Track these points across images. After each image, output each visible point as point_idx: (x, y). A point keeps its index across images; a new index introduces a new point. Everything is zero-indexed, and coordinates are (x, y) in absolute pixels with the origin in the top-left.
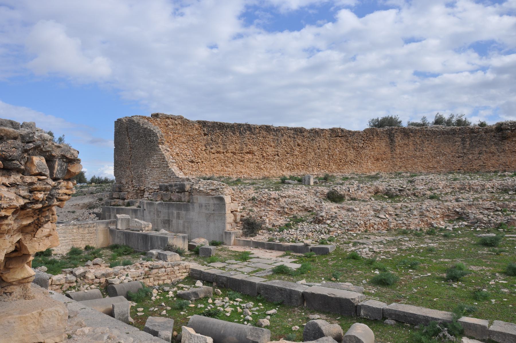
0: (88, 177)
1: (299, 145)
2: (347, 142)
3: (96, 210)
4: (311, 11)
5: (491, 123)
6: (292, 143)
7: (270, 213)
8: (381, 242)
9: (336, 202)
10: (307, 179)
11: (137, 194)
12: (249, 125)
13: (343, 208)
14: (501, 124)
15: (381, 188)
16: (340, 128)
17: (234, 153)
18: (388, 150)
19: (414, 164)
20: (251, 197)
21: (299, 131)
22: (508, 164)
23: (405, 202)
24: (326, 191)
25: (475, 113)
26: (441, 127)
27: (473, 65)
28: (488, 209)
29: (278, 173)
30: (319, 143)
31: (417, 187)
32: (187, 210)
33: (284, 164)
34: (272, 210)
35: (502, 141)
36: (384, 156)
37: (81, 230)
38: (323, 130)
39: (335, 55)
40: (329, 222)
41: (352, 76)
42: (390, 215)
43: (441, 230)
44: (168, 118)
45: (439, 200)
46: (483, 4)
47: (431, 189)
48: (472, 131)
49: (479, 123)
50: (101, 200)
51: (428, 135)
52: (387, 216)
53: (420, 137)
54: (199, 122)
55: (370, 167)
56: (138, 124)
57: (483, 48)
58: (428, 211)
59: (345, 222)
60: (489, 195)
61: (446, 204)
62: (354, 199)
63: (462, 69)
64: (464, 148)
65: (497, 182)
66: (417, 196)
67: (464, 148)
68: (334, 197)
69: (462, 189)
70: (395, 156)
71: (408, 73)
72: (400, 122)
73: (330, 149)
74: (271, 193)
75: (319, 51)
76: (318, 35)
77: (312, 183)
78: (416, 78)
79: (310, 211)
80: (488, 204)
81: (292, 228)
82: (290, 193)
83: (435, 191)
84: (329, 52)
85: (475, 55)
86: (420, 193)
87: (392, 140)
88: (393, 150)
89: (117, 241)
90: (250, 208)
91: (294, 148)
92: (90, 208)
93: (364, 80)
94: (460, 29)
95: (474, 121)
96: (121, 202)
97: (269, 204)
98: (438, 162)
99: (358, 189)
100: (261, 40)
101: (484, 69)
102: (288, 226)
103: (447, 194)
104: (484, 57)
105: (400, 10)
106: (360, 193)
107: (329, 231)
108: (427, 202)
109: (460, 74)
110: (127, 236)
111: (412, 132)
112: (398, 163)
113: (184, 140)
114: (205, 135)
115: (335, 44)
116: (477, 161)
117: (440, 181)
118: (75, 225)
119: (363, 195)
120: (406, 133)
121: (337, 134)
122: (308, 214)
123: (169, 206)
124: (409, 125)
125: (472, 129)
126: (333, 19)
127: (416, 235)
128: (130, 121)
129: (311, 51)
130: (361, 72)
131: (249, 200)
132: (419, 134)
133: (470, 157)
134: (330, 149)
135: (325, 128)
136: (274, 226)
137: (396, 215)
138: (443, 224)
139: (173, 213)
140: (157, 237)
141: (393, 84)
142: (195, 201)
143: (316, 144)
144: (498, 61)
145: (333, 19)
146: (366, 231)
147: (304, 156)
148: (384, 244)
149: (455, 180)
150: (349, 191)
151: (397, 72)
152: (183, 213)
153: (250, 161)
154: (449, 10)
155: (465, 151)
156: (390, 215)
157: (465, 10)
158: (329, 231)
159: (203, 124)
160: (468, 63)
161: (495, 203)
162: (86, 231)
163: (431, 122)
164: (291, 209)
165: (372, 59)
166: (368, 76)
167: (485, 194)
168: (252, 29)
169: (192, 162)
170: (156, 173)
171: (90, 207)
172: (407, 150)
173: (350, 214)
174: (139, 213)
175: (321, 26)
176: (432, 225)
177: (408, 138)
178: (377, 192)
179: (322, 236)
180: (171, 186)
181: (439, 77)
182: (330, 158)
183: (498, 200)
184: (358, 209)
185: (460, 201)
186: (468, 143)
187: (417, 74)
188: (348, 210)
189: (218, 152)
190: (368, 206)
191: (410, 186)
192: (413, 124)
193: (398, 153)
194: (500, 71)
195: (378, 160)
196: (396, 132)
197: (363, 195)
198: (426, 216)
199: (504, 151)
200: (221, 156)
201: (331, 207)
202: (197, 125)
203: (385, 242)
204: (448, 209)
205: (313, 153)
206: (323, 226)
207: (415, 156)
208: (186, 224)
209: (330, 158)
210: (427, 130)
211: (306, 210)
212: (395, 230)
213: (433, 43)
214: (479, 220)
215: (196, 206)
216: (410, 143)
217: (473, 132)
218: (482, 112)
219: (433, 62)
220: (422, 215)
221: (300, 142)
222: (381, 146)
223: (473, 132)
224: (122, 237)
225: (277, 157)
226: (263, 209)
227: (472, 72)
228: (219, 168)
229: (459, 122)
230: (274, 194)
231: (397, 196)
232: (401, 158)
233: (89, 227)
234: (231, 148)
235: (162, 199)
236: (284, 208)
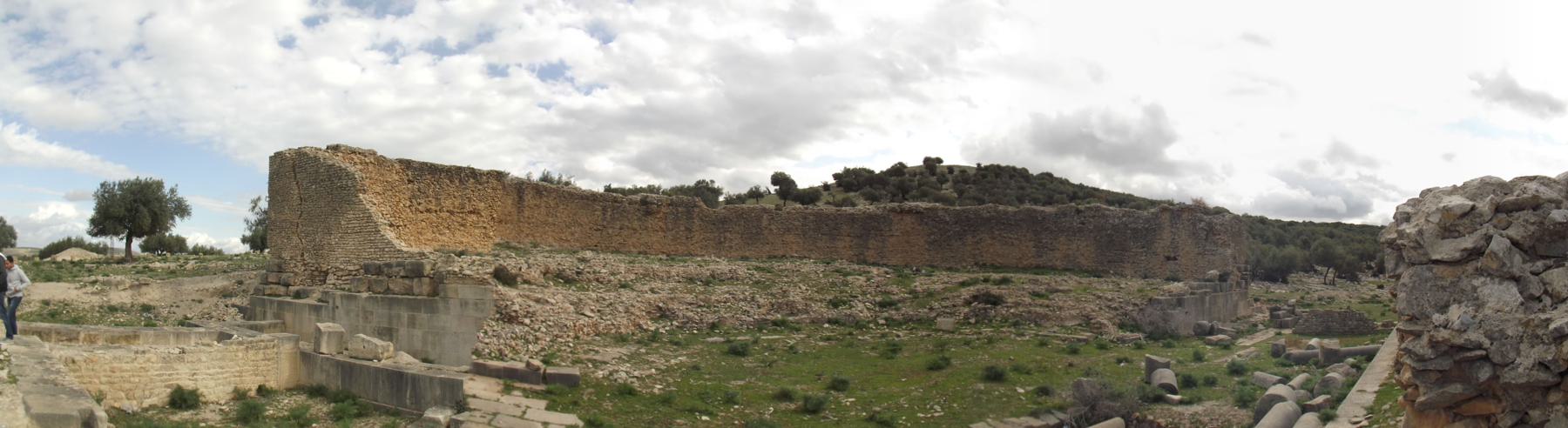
0: (190, 244)
3: (237, 301)
11: (312, 277)
17: (452, 213)
18: (514, 210)
32: (433, 310)
37: (251, 352)
40: (527, 321)
44: (354, 152)
50: (240, 283)
54: (401, 161)
56: (316, 159)
88: (520, 211)
89: (319, 378)
92: (225, 296)
96: (282, 289)
107: (537, 339)
110: (347, 370)
113: (378, 189)
114: (410, 181)
118: (240, 343)
123: (391, 303)
128: (300, 154)
139: (399, 316)
140: (431, 379)
142: (450, 294)
152: (423, 316)
153: (474, 225)
159: (407, 164)
162: (261, 356)
170: (351, 243)
171: (225, 294)
174: (323, 312)
180: (389, 265)
189: (428, 211)
194: (568, 113)
200: (433, 216)
202: (397, 166)
207: (546, 223)
208: (430, 338)
215: (454, 305)
224: (332, 371)
228: (429, 235)
233: (266, 347)
234: (447, 204)
235: (369, 289)
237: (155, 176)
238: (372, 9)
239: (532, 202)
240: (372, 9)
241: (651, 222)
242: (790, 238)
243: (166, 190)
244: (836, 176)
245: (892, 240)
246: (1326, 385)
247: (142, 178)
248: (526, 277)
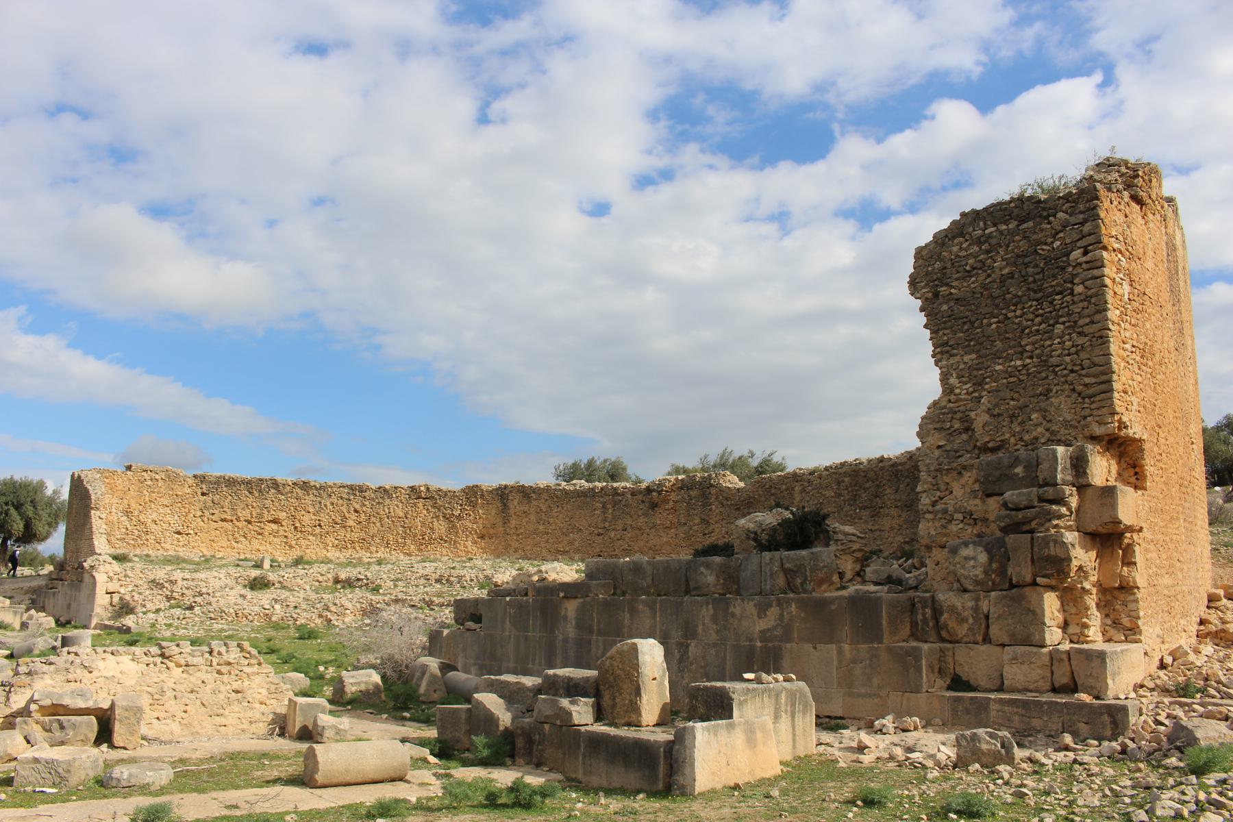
1: (356, 511)
2: (433, 507)
6: (344, 509)
12: (523, 486)
21: (358, 490)
33: (330, 540)
36: (492, 531)
46: (910, 127)
64: (605, 520)
75: (885, 215)
88: (506, 522)
98: (571, 543)
100: (724, 188)
114: (203, 494)
133: (612, 534)
153: (274, 534)
155: (607, 525)
168: (690, 154)
169: (179, 533)
177: (530, 502)
178: (337, 581)
200: (229, 526)
202: (190, 481)
205: (378, 524)
207: (536, 532)
221: (358, 507)
223: (618, 494)
225: (318, 530)
228: (224, 543)
234: (245, 514)
237: (33, 476)
238: (756, 160)
239: (520, 508)
240: (756, 160)
241: (661, 517)
243: (49, 492)
247: (17, 478)
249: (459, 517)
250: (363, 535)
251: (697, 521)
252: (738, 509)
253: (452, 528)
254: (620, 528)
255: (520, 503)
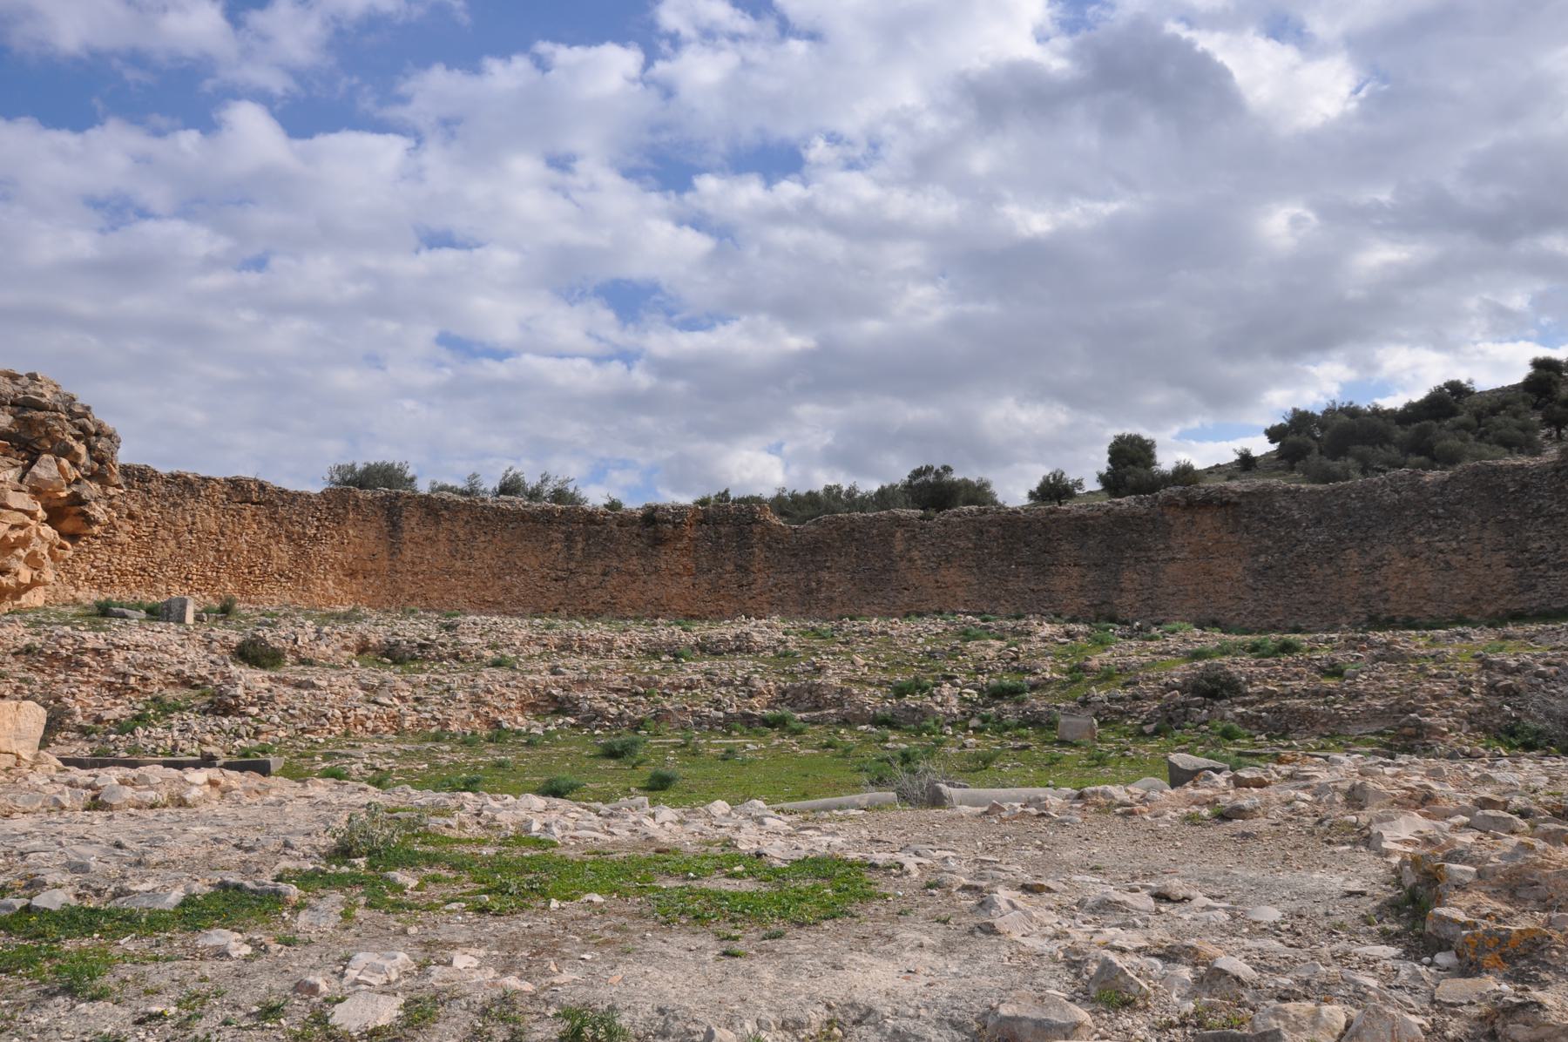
1: (131, 516)
2: (271, 519)
4: (131, 75)
5: (633, 505)
7: (83, 688)
8: (389, 754)
9: (263, 667)
10: (176, 607)
13: (283, 681)
14: (655, 509)
15: (373, 640)
16: (255, 480)
19: (448, 591)
20: (21, 644)
22: (664, 601)
23: (436, 672)
24: (236, 639)
25: (598, 475)
26: (520, 501)
27: (600, 339)
28: (617, 691)
29: (62, 593)
30: (193, 516)
31: (463, 639)
33: (82, 568)
34: (88, 682)
35: (653, 547)
36: (369, 565)
38: (206, 480)
39: (198, 240)
40: (254, 710)
41: (248, 316)
42: (403, 699)
43: (519, 733)
45: (513, 668)
47: (494, 647)
48: (591, 518)
49: (607, 502)
51: (486, 519)
52: (396, 701)
53: (467, 522)
55: (331, 592)
57: (631, 299)
58: (489, 692)
59: (296, 712)
60: (621, 662)
61: (530, 677)
62: (309, 663)
63: (567, 348)
64: (569, 558)
65: (638, 633)
66: (462, 661)
67: (569, 558)
68: (253, 654)
69: (565, 646)
70: (399, 566)
71: (423, 335)
72: (412, 480)
73: (223, 534)
74: (85, 635)
75: (144, 214)
76: (143, 161)
77: (190, 618)
78: (444, 354)
79: (196, 687)
80: (617, 681)
81: (153, 726)
82: (138, 637)
83: (505, 651)
84: (178, 227)
85: (608, 316)
86: (469, 653)
87: (394, 525)
88: (394, 551)
90: (22, 675)
91: (118, 523)
93: (285, 336)
94: (575, 236)
95: (595, 497)
97: (80, 665)
98: (507, 590)
99: (319, 638)
101: (627, 357)
102: (140, 719)
103: (531, 657)
104: (631, 326)
105: (419, 142)
106: (323, 648)
107: (258, 732)
108: (486, 673)
109: (568, 361)
111: (447, 508)
112: (407, 588)
115: (202, 202)
116: (598, 591)
117: (518, 629)
119: (330, 652)
120: (435, 508)
121: (244, 493)
122: (193, 693)
124: (433, 491)
125: (590, 514)
126: (205, 120)
127: (464, 742)
129: (115, 210)
130: (279, 308)
131: (14, 654)
132: (465, 516)
134: (223, 534)
135: (213, 475)
136: (99, 720)
137: (417, 700)
138: (522, 722)
141: (374, 361)
143: (184, 519)
144: (665, 342)
145: (205, 120)
146: (347, 734)
147: (146, 548)
148: (396, 758)
149: (549, 627)
150: (295, 641)
151: (391, 327)
154: (554, 176)
155: (572, 565)
156: (403, 699)
157: (593, 187)
158: (258, 732)
160: (589, 334)
161: (632, 679)
163: (490, 489)
164: (144, 679)
165: (320, 273)
166: (298, 325)
167: (615, 661)
172: (433, 555)
173: (306, 693)
175: (159, 133)
176: (498, 724)
177: (438, 523)
179: (239, 742)
181: (511, 360)
182: (220, 561)
183: (638, 671)
184: (324, 683)
185: (561, 673)
186: (580, 546)
187: (447, 341)
188: (299, 685)
190: (349, 679)
191: (445, 637)
192: (443, 488)
193: (408, 559)
194: (667, 368)
195: (352, 574)
196: (406, 505)
197: (330, 652)
198: (485, 704)
199: (657, 570)
201: (250, 680)
203: (397, 753)
204: (535, 691)
205: (172, 543)
206: (239, 720)
207: (451, 572)
209: (220, 561)
210: (484, 508)
211: (187, 683)
212: (414, 733)
213: (502, 258)
214: (599, 714)
216: (441, 536)
217: (593, 522)
218: (615, 474)
219: (497, 314)
220: (477, 701)
221: (136, 507)
222: (360, 537)
223: (593, 522)
226: (62, 676)
227: (598, 360)
229: (559, 495)
230: (92, 639)
231: (414, 659)
232: (416, 574)
236: (125, 675)
241: (667, 559)
242: (950, 575)
244: (1273, 434)
245: (1172, 569)
246: (698, 724)
248: (304, 653)
249: (314, 539)
250: (141, 560)
251: (730, 567)
252: (795, 555)
253: (301, 556)
254: (598, 571)
255: (421, 523)
